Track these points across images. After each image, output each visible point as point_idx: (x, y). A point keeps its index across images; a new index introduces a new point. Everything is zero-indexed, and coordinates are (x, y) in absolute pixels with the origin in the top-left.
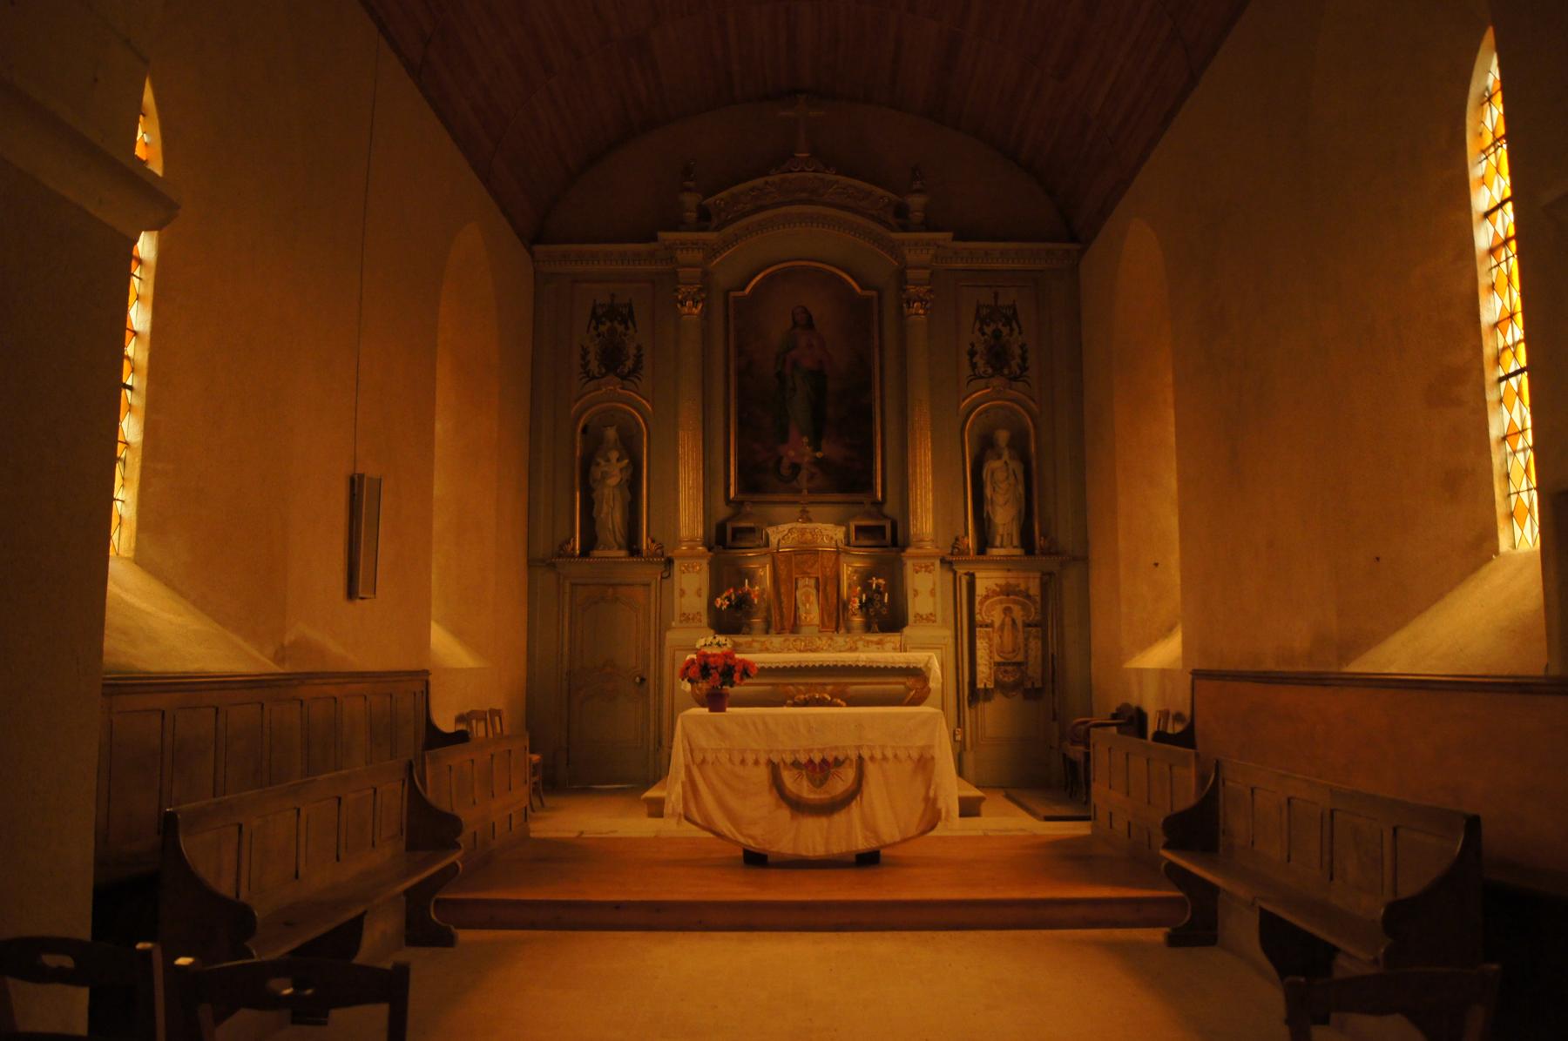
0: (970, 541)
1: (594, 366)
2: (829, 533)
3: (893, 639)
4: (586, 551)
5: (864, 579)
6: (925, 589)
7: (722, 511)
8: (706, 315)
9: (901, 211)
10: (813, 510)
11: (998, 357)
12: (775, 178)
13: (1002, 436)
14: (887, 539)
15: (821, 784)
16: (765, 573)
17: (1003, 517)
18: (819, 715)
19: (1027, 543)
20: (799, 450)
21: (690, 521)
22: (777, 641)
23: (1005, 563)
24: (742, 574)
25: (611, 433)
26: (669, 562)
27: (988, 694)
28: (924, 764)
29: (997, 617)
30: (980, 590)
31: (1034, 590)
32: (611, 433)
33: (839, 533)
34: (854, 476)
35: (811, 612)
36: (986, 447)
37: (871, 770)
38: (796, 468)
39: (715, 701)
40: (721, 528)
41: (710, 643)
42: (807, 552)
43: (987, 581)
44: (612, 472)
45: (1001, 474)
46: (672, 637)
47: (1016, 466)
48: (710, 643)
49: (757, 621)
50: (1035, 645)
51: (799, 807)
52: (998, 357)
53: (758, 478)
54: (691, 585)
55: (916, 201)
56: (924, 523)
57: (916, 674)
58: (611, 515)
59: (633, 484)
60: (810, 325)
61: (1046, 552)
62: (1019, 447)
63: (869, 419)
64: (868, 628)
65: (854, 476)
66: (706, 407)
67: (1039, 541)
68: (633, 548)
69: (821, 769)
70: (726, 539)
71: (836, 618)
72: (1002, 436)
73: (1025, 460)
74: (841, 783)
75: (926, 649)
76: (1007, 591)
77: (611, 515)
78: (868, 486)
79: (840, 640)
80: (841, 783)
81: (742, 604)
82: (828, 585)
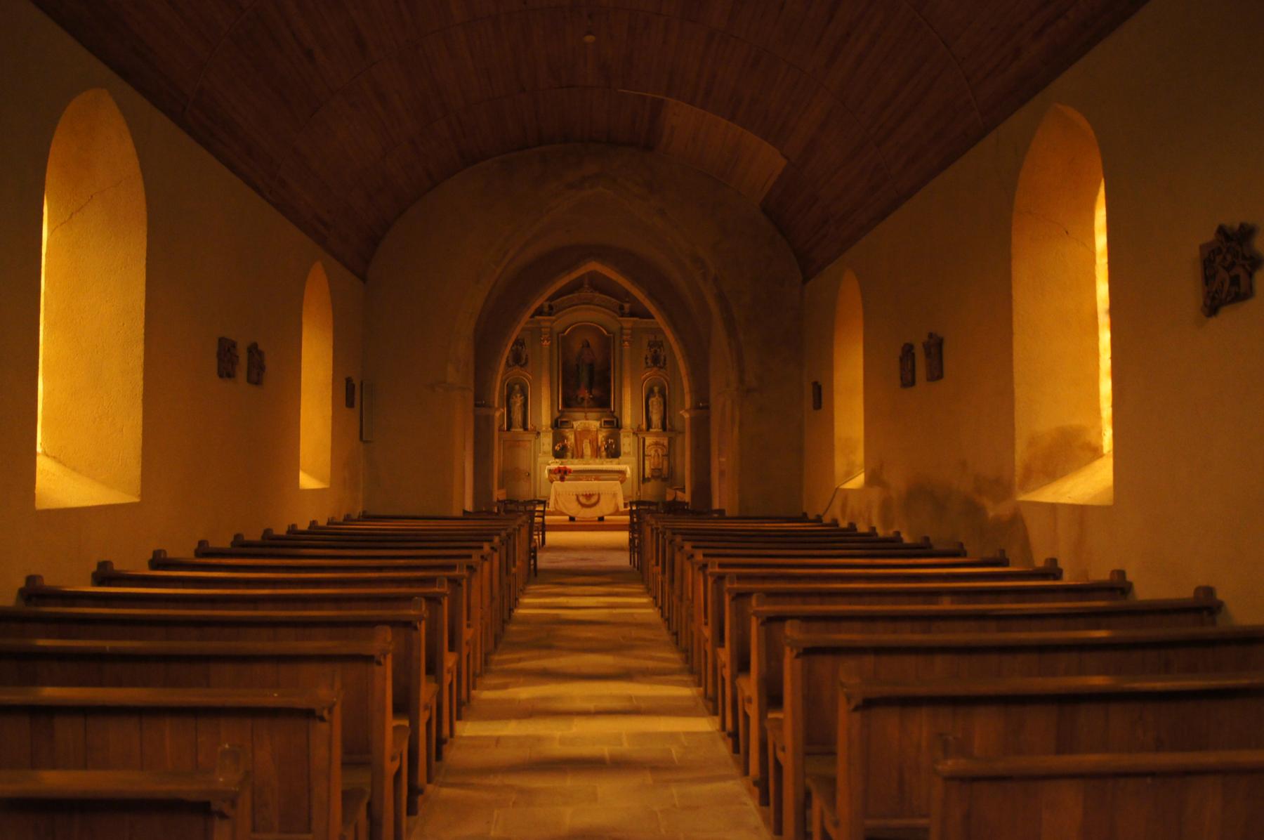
0: (644, 426)
1: (511, 362)
2: (594, 424)
3: (616, 460)
4: (508, 429)
5: (607, 438)
6: (627, 443)
7: (557, 414)
8: (551, 345)
9: (622, 308)
10: (589, 415)
11: (655, 360)
12: (576, 295)
13: (656, 389)
14: (614, 425)
15: (589, 500)
16: (571, 437)
17: (656, 418)
18: (44, 408)
19: (664, 428)
20: (584, 394)
21: (545, 419)
22: (576, 461)
23: (657, 434)
24: (564, 438)
25: (517, 387)
26: (538, 433)
27: (649, 480)
28: (615, 495)
29: (653, 453)
30: (647, 443)
31: (666, 442)
32: (517, 387)
33: (597, 424)
34: (603, 402)
35: (588, 450)
36: (650, 393)
37: (602, 498)
38: (583, 399)
39: (562, 479)
40: (556, 421)
41: (555, 464)
42: (586, 431)
43: (649, 440)
44: (518, 401)
45: (655, 401)
46: (540, 460)
47: (661, 400)
48: (555, 464)
49: (569, 454)
50: (666, 463)
51: (583, 506)
52: (655, 360)
53: (569, 402)
54: (546, 441)
55: (627, 306)
56: (627, 420)
57: (622, 472)
58: (518, 416)
59: (525, 405)
60: (588, 345)
61: (671, 430)
62: (662, 393)
63: (609, 381)
64: (607, 457)
65: (603, 402)
66: (551, 377)
67: (668, 426)
68: (525, 429)
69: (588, 496)
70: (558, 425)
71: (596, 453)
72: (656, 389)
73: (664, 396)
74: (594, 500)
75: (626, 465)
76: (656, 444)
77: (518, 416)
78: (609, 406)
79: (598, 461)
80: (594, 500)
81: (564, 448)
82: (594, 442)
